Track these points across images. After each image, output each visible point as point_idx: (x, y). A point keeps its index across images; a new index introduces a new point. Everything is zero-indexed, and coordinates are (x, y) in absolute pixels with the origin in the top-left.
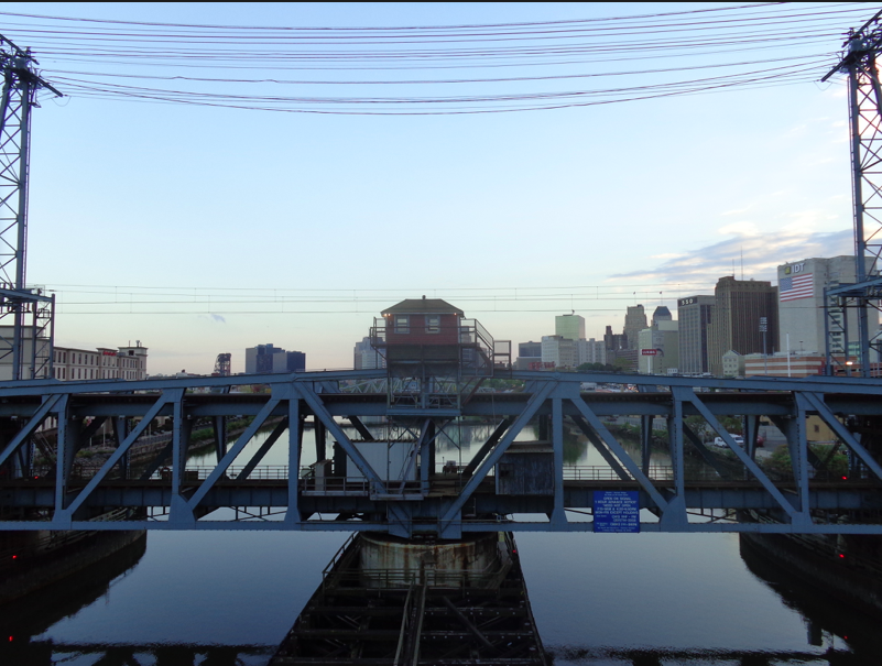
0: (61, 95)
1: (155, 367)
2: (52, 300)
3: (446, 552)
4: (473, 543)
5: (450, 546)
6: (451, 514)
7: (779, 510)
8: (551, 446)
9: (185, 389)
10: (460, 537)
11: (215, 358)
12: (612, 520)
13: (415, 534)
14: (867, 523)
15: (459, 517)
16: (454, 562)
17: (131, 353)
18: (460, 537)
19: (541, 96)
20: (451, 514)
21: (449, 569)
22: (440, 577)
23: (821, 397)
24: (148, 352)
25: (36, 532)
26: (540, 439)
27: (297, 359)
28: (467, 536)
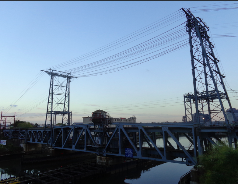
0: (77, 78)
1: (138, 121)
2: (71, 112)
3: (103, 158)
4: (109, 157)
5: (104, 157)
6: (104, 151)
7: (160, 156)
8: (118, 138)
9: (74, 127)
10: (105, 155)
11: (182, 117)
12: (128, 155)
13: (106, 155)
14: (79, 151)
15: (105, 152)
16: (105, 160)
17: (133, 118)
18: (105, 155)
19: (94, 67)
20: (104, 151)
21: (104, 162)
22: (102, 163)
23: (167, 128)
24: (137, 118)
25: (69, 150)
26: (162, 138)
27: (37, 125)
28: (107, 156)
